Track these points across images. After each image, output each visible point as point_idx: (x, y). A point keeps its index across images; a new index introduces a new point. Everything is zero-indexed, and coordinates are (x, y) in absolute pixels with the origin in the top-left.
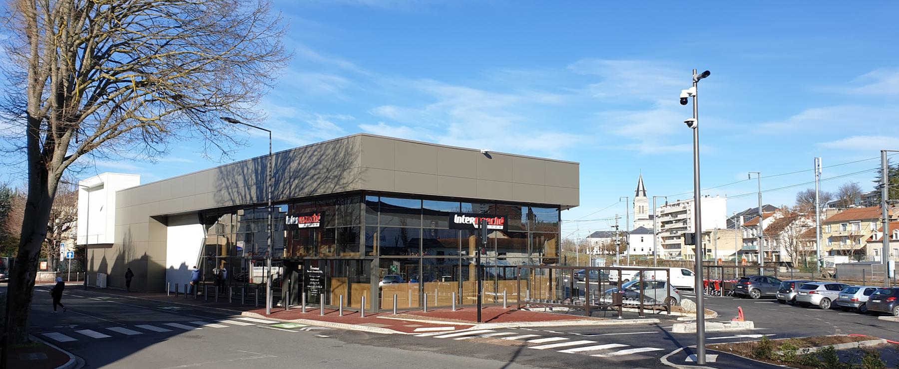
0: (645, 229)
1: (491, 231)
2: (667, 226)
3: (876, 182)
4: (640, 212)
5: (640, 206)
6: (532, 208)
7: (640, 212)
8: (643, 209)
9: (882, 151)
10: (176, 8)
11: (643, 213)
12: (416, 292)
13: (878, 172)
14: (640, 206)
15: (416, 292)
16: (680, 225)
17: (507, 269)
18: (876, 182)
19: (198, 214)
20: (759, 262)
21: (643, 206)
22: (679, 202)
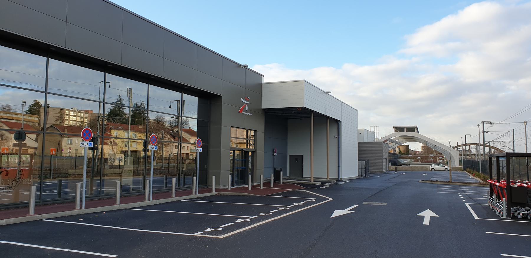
20: (390, 164)
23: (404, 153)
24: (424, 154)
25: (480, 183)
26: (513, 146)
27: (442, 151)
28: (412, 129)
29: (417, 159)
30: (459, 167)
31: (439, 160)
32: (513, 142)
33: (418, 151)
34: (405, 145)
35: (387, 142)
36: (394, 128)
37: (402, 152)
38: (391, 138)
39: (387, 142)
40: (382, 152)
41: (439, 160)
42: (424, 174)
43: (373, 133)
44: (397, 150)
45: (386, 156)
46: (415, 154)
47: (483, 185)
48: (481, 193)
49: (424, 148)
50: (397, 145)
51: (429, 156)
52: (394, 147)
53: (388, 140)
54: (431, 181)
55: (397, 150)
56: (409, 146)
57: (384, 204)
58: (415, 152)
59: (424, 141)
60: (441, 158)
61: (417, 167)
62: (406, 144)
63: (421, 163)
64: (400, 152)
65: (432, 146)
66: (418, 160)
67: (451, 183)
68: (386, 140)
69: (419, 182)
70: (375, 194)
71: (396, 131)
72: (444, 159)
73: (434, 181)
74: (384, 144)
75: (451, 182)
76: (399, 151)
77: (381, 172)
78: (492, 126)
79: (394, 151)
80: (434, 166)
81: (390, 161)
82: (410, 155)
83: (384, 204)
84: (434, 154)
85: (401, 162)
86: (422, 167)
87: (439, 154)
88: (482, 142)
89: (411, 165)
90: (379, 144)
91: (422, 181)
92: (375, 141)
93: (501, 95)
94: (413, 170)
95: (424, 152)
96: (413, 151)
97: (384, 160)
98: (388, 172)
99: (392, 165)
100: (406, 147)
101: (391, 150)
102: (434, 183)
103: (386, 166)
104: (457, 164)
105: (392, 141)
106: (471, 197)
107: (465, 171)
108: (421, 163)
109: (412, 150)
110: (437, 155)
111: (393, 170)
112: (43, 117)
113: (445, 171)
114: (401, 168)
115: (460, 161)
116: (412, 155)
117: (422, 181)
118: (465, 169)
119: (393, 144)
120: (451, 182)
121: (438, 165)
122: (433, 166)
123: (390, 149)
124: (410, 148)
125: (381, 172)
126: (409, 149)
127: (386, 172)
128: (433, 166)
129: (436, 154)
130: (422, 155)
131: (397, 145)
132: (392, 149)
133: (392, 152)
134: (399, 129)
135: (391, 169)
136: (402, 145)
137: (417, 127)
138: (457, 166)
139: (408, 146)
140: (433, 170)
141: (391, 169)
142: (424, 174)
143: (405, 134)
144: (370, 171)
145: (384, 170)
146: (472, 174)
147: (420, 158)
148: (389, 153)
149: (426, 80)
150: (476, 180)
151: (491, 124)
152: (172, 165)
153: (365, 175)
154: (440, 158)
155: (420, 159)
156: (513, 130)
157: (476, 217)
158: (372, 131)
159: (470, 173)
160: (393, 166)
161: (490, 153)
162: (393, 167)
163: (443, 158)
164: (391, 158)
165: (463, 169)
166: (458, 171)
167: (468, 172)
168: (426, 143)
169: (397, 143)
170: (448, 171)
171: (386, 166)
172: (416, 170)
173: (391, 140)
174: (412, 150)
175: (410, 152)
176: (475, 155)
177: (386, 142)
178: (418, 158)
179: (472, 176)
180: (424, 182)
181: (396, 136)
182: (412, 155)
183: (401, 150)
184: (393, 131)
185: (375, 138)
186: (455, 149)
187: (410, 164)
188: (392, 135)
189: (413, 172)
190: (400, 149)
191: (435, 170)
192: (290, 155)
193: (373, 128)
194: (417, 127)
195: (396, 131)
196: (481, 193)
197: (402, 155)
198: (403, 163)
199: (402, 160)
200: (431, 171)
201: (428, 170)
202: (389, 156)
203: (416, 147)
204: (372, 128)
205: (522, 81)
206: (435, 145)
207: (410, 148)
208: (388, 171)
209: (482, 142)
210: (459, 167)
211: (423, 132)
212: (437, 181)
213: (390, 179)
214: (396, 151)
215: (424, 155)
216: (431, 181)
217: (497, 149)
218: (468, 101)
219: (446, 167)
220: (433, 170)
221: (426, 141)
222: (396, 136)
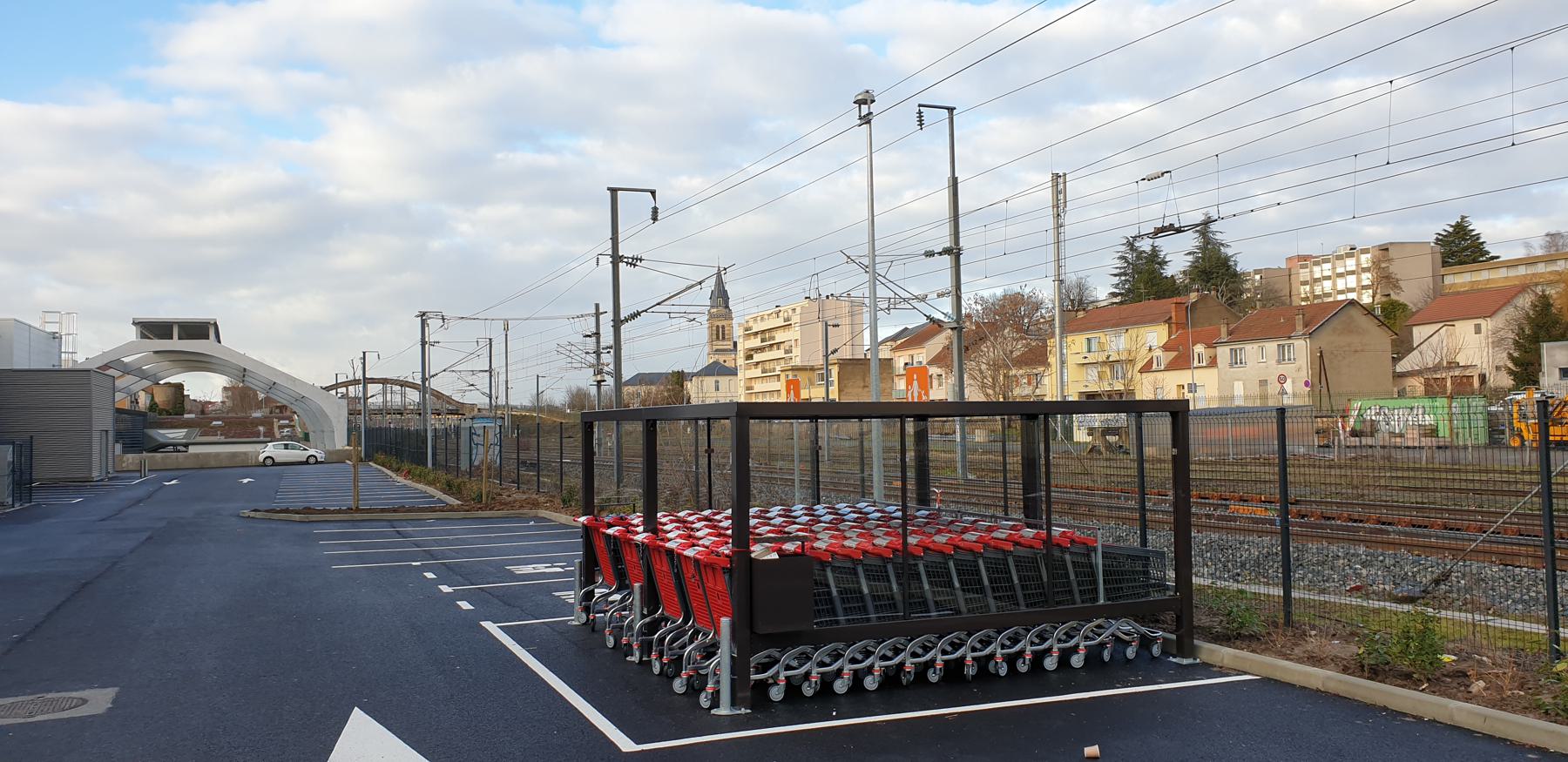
0: (727, 367)
1: (1540, 526)
2: (757, 357)
3: (1115, 275)
4: (718, 338)
5: (718, 327)
6: (623, 380)
7: (718, 338)
8: (723, 331)
9: (614, 191)
10: (861, 364)
11: (724, 338)
12: (1555, 296)
13: (1119, 258)
14: (718, 327)
15: (1555, 296)
16: (780, 353)
17: (711, 421)
18: (1115, 275)
19: (1445, 264)
20: (118, 447)
21: (723, 327)
22: (778, 309)
23: (167, 408)
24: (231, 410)
25: (452, 509)
26: (488, 385)
27: (293, 401)
28: (198, 330)
29: (212, 428)
30: (347, 448)
31: (282, 427)
32: (488, 374)
33: (210, 403)
34: (169, 383)
35: (110, 372)
36: (134, 323)
37: (161, 407)
38: (126, 360)
39: (110, 372)
40: (89, 407)
41: (282, 427)
42: (245, 481)
43: (55, 337)
44: (143, 400)
45: (103, 421)
46: (203, 412)
47: (461, 514)
48: (500, 552)
49: (230, 393)
50: (146, 383)
51: (247, 418)
52: (134, 388)
53: (111, 367)
54: (287, 511)
55: (143, 400)
56: (182, 385)
57: (99, 700)
58: (203, 407)
59: (237, 367)
60: (287, 422)
61: (217, 455)
62: (173, 380)
63: (222, 439)
64: (153, 406)
65: (262, 385)
66: (215, 431)
67: (358, 516)
68: (107, 366)
69: (238, 516)
70: (50, 615)
71: (144, 336)
72: (294, 426)
73: (297, 512)
74: (95, 380)
75: (358, 510)
76: (148, 402)
77: (81, 484)
78: (446, 326)
79: (132, 402)
80: (272, 449)
81: (119, 437)
82: (186, 416)
83: (99, 700)
84: (264, 409)
85: (156, 440)
86: (234, 455)
87: (278, 411)
88: (359, 375)
89: (192, 450)
90: (80, 377)
91: (252, 514)
92: (63, 367)
93: (436, 244)
94: (203, 466)
95: (229, 403)
96: (195, 401)
97: (96, 437)
98: (110, 479)
99: (126, 449)
100: (173, 389)
101: (122, 400)
102: (297, 517)
103: (104, 455)
104: (340, 442)
105: (127, 370)
106: (440, 565)
107: (370, 461)
108: (222, 439)
109: (191, 398)
110: (271, 413)
111: (131, 468)
112: (820, 469)
113: (307, 463)
114: (160, 460)
115: (351, 430)
116: (193, 416)
117: (252, 514)
118: (369, 457)
119: (129, 379)
120: (358, 510)
121: (286, 447)
122: (271, 450)
123: (118, 396)
124: (186, 393)
125: (81, 484)
126: (184, 396)
127: (102, 480)
128: (271, 450)
129: (268, 410)
130: (224, 415)
131: (146, 383)
132: (125, 395)
133: (127, 405)
134: (153, 329)
135: (124, 465)
136: (161, 382)
137: (215, 324)
138: (339, 447)
139: (180, 387)
140: (269, 462)
141: (124, 465)
142: (245, 481)
143: (175, 344)
144: (37, 480)
145: (95, 474)
146: (397, 471)
147: (220, 423)
148: (119, 411)
149: (230, 180)
150: (421, 492)
151: (443, 319)
152: (1531, 313)
153: (10, 500)
154: (281, 422)
155: (220, 426)
156: (490, 339)
157: (626, 744)
158: (50, 328)
159: (390, 468)
160: (130, 456)
161: (1121, 397)
162: (131, 459)
163: (292, 424)
164: (122, 426)
165: (363, 455)
166: (348, 461)
167: (383, 466)
168: (244, 376)
169: (143, 375)
170: (317, 462)
171: (104, 455)
172: (213, 463)
173: (126, 365)
174: (191, 398)
175: (187, 406)
176: (379, 411)
177: (105, 372)
178: (214, 423)
179: (401, 480)
180: (258, 515)
181: (142, 353)
182: (193, 416)
183: (157, 400)
184: (132, 334)
185: (63, 355)
186: (333, 392)
187: (186, 445)
188: (129, 348)
189: (203, 471)
190: (153, 397)
191: (275, 464)
192: (1560, 369)
193: (56, 318)
194: (215, 323)
195: (144, 336)
196: (500, 552)
197: (160, 414)
198: (162, 440)
199: (162, 431)
200: (264, 464)
201: (254, 463)
202: (116, 421)
203: (206, 388)
204: (49, 318)
205: (486, 212)
206: (275, 383)
207: (186, 393)
208: (110, 475)
209: (359, 375)
210: (347, 448)
211: (234, 341)
212: (308, 510)
213: (120, 511)
214: (137, 403)
215: (230, 415)
216: (287, 511)
217: (436, 393)
218: (354, 256)
219: (312, 452)
220: (269, 462)
221: (245, 370)
222: (142, 353)
